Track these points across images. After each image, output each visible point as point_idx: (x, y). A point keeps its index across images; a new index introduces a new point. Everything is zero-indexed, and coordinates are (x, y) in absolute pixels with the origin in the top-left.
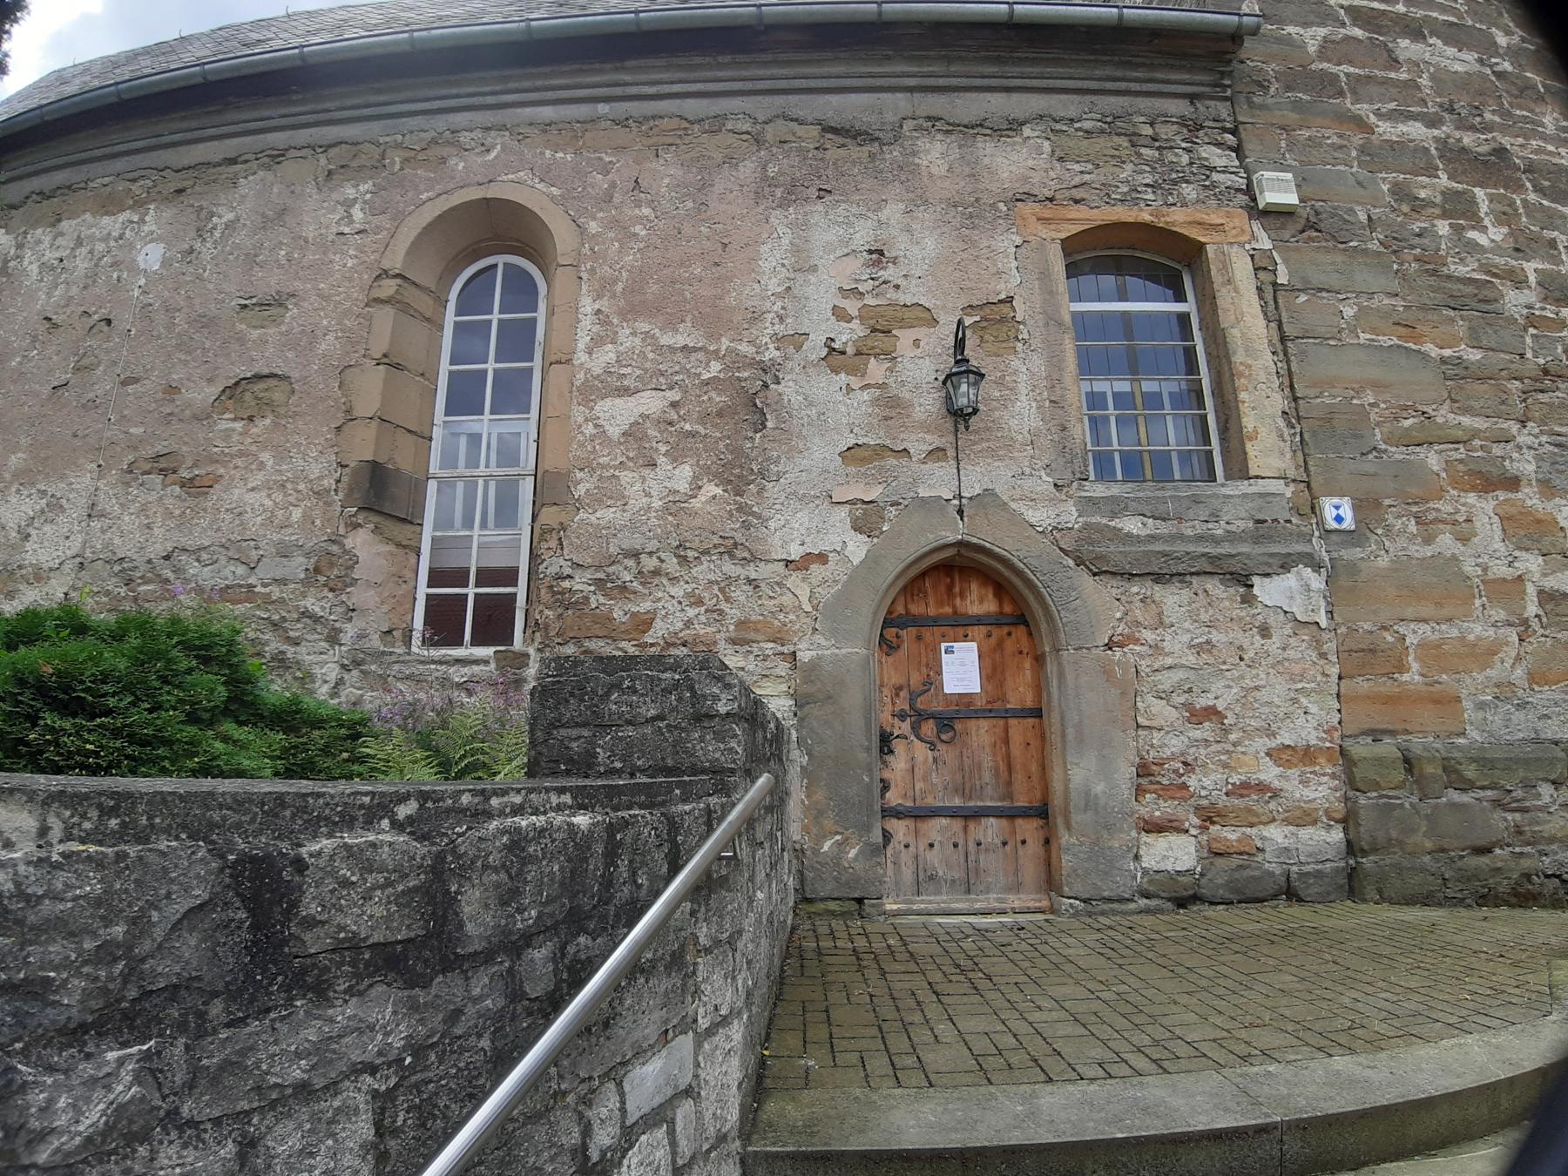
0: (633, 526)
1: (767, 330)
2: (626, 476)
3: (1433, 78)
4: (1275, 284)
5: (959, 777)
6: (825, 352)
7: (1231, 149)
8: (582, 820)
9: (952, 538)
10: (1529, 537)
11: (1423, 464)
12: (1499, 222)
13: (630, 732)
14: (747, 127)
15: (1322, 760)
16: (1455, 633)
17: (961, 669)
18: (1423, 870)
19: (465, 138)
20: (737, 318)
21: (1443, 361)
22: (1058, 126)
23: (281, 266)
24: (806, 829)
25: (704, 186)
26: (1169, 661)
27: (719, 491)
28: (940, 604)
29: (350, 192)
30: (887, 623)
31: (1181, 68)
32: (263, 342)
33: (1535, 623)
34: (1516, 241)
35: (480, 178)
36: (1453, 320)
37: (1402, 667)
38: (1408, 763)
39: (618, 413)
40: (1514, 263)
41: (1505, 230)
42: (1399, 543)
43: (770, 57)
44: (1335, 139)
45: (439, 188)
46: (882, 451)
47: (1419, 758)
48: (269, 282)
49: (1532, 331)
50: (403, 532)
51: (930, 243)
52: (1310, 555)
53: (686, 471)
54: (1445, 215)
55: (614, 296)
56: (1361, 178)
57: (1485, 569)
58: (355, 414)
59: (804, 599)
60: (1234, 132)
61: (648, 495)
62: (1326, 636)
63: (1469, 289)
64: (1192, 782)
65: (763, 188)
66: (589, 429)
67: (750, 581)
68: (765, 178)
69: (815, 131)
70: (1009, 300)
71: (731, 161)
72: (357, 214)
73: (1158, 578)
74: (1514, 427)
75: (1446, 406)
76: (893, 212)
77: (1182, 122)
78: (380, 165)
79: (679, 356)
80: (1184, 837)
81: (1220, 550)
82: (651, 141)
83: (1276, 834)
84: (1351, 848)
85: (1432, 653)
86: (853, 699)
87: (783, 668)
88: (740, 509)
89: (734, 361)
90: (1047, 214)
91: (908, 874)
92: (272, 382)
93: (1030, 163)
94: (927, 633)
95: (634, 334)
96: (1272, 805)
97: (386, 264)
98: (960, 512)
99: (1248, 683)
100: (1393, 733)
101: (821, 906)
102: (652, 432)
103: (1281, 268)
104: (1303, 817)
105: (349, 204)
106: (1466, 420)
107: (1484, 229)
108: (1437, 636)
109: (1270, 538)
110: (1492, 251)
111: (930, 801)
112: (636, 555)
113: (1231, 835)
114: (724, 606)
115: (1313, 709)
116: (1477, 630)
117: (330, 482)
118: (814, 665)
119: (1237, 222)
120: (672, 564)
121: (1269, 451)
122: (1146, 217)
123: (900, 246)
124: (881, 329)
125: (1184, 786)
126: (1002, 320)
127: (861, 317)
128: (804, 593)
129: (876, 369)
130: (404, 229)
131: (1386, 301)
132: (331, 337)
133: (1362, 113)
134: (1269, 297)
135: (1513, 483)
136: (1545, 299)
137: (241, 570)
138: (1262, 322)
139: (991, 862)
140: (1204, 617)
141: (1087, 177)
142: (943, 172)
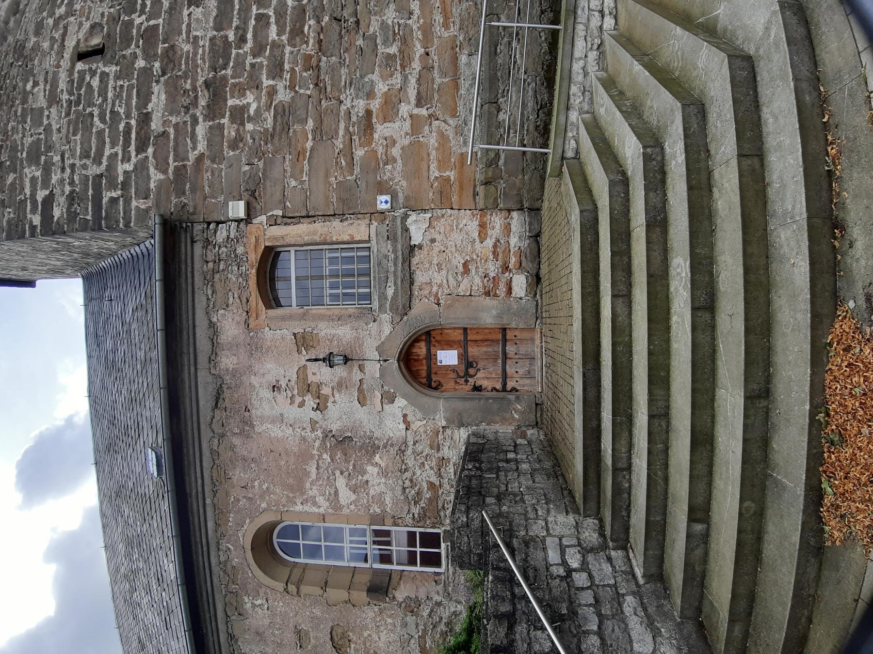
0: (393, 490)
1: (308, 433)
2: (372, 492)
3: (171, 114)
4: (283, 217)
5: (491, 361)
6: (318, 412)
7: (217, 226)
8: (490, 578)
9: (396, 365)
10: (393, 108)
11: (361, 158)
12: (244, 95)
13: (472, 544)
14: (216, 441)
15: (485, 219)
16: (434, 152)
17: (448, 357)
18: (530, 179)
19: (222, 559)
20: (304, 447)
21: (314, 139)
22: (211, 306)
23: (283, 633)
24: (510, 424)
25: (244, 459)
26: (445, 281)
27: (378, 456)
28: (422, 365)
29: (249, 605)
30: (430, 386)
31: (179, 248)
32: (316, 638)
33: (431, 111)
34: (253, 87)
35: (242, 552)
36: (294, 131)
37: (448, 179)
38: (486, 183)
39: (346, 496)
40: (264, 91)
41: (248, 92)
42: (395, 173)
43: (184, 432)
44: (209, 174)
45: (247, 569)
46: (360, 390)
47: (485, 178)
48: (290, 636)
49: (297, 88)
50: (395, 578)
51: (269, 366)
52: (402, 218)
53: (369, 468)
54: (243, 124)
55: (295, 497)
56: (228, 165)
57: (407, 134)
58: (347, 599)
59: (422, 423)
60: (209, 223)
61: (380, 483)
62: (435, 215)
63: (279, 118)
64: (492, 275)
65: (245, 435)
66: (352, 507)
67: (414, 444)
68: (240, 434)
69: (217, 412)
70: (294, 334)
71: (232, 448)
72: (259, 602)
73: (412, 283)
74: (343, 108)
75: (335, 142)
76: (255, 380)
77: (205, 247)
78: (236, 594)
79: (321, 471)
80: (513, 279)
81: (400, 257)
82: (223, 481)
83: (514, 241)
84: (521, 209)
85: (443, 164)
86: (459, 405)
87: (449, 432)
88: (385, 447)
89: (323, 448)
90: (254, 315)
91: (527, 381)
92: (334, 633)
93: (230, 320)
94: (433, 371)
95: (311, 489)
96: (502, 242)
97: (282, 590)
98: (385, 361)
99: (454, 249)
100: (475, 186)
101: (539, 419)
102: (354, 482)
103: (275, 212)
104: (507, 229)
105: (254, 606)
106: (341, 132)
107: (249, 104)
108: (435, 161)
109: (395, 234)
110: (259, 102)
111: (500, 372)
112: (404, 489)
113: (513, 260)
114: (424, 454)
115: (464, 222)
116: (433, 141)
117: (376, 609)
118: (447, 420)
119: (254, 230)
120: (408, 475)
121: (359, 230)
122: (254, 271)
123: (271, 378)
124: (307, 388)
125: (494, 278)
126: (304, 338)
127: (303, 396)
128: (419, 423)
129: (326, 391)
130: (266, 583)
131: (287, 163)
132: (314, 611)
133: (194, 157)
134: (289, 221)
135: (369, 113)
136: (281, 77)
137: (412, 641)
138: (300, 226)
139: (522, 350)
140: (427, 266)
141: (236, 296)
142: (236, 358)
